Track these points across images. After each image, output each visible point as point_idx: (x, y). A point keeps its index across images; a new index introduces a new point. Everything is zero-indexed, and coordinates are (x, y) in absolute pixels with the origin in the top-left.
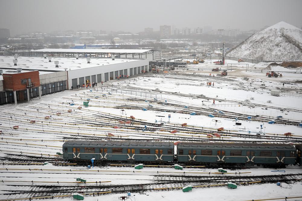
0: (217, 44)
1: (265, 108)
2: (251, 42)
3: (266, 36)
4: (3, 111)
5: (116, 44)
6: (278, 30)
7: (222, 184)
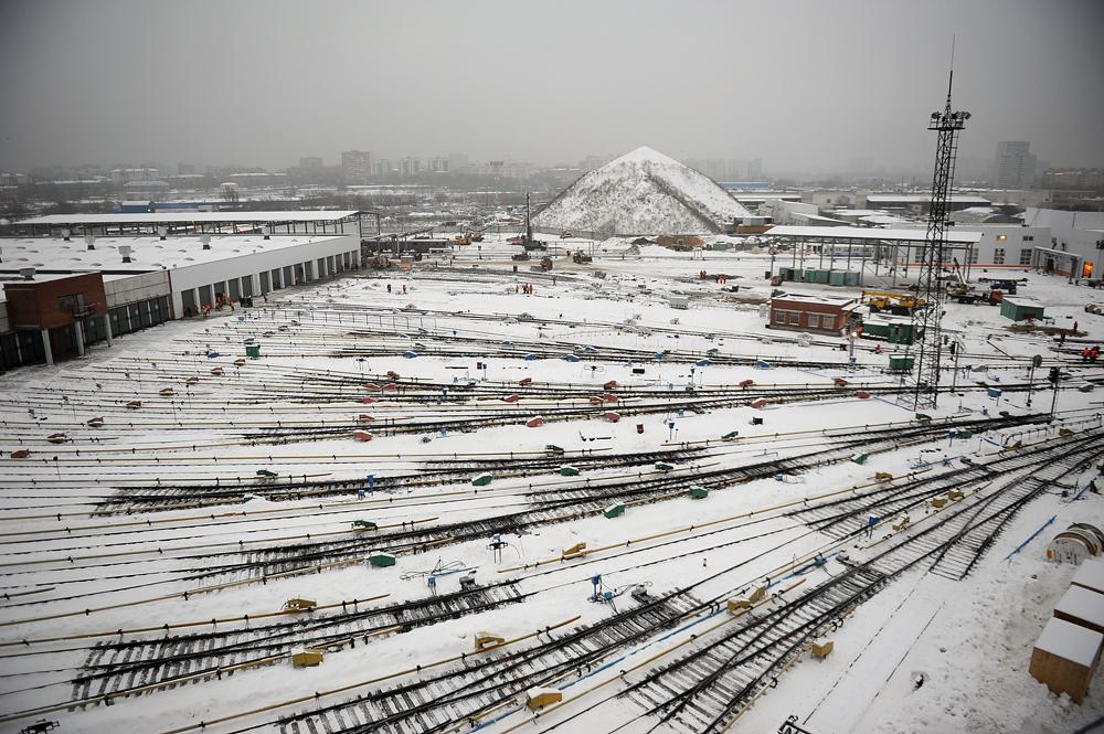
0: (492, 196)
1: (672, 335)
2: (582, 192)
3: (614, 178)
4: (28, 385)
5: (241, 200)
6: (639, 166)
7: (674, 492)
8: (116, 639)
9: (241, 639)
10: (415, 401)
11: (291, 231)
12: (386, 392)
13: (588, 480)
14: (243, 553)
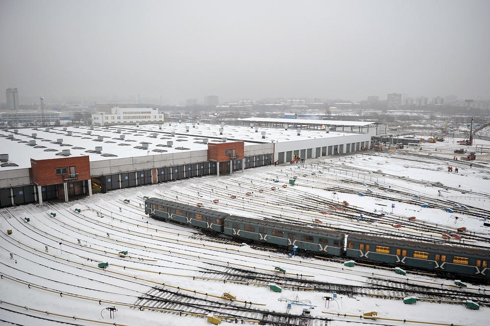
0: (463, 119)
4: (205, 183)
5: (332, 115)
8: (161, 287)
9: (201, 303)
10: (348, 217)
11: (361, 131)
12: (337, 211)
13: (408, 279)
14: (227, 267)
